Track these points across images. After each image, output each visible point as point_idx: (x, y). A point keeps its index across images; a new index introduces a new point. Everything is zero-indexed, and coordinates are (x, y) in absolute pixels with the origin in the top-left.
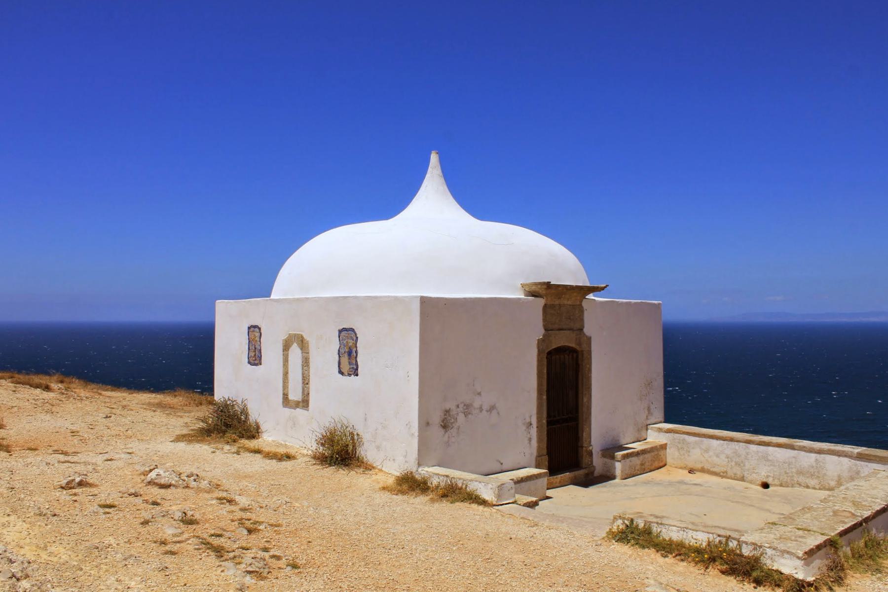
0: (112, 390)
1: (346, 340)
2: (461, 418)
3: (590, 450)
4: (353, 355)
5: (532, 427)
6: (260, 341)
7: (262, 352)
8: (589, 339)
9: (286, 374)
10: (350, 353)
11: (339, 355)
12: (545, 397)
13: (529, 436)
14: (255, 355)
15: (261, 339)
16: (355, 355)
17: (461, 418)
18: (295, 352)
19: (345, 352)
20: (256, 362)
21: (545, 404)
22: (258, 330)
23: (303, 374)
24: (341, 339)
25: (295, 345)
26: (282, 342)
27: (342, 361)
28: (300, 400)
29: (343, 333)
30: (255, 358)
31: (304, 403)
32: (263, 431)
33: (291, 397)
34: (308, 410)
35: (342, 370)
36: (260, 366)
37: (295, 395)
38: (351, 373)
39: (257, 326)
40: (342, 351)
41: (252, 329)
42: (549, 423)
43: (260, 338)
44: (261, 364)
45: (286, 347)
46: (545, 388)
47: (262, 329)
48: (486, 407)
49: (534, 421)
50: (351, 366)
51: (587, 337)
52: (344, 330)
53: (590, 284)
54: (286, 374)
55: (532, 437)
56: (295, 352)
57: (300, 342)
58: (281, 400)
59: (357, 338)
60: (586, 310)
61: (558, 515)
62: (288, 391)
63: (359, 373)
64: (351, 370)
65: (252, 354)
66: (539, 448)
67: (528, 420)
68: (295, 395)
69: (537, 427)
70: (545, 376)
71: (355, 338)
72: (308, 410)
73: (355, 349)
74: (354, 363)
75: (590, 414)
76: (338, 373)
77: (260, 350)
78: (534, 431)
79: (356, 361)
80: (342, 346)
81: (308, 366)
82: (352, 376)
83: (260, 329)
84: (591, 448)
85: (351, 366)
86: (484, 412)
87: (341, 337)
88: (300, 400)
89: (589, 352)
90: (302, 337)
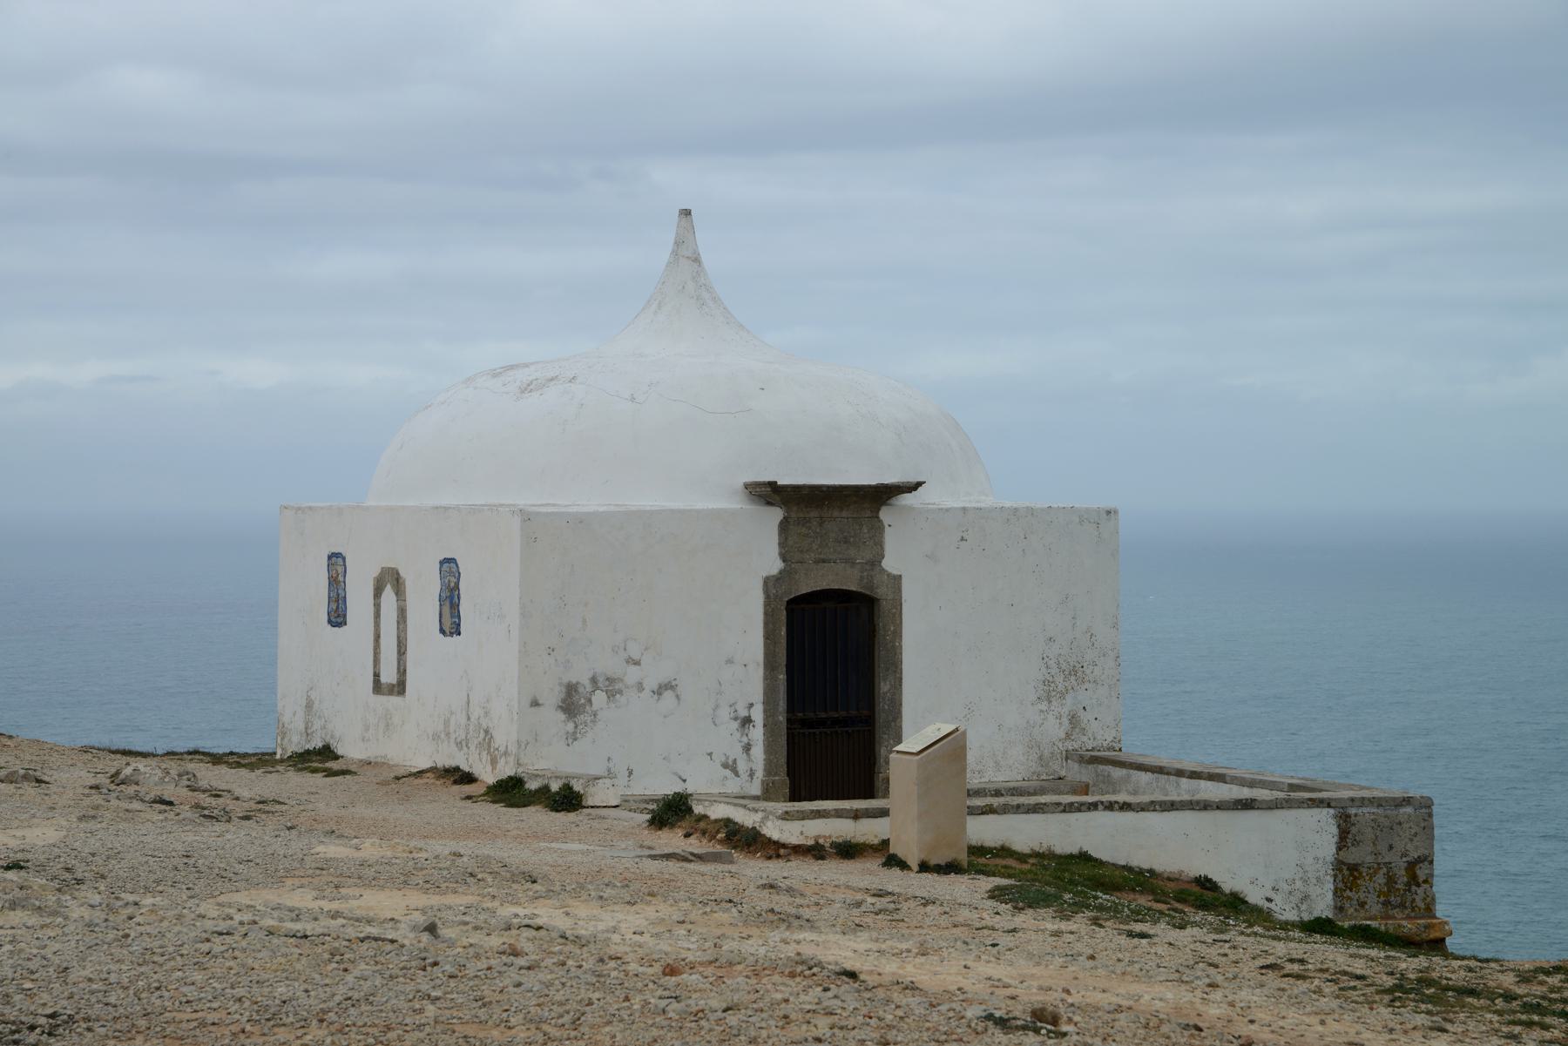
2: (599, 698)
5: (754, 726)
6: (345, 582)
8: (897, 579)
9: (377, 637)
10: (451, 597)
12: (782, 677)
13: (745, 740)
14: (338, 607)
17: (599, 698)
18: (389, 595)
20: (339, 620)
22: (340, 560)
23: (398, 637)
26: (372, 583)
27: (443, 611)
28: (395, 682)
30: (337, 618)
31: (400, 688)
32: (584, 804)
33: (384, 679)
36: (345, 627)
37: (389, 676)
39: (340, 554)
41: (334, 559)
43: (345, 576)
44: (345, 624)
45: (378, 592)
46: (782, 659)
47: (347, 560)
48: (651, 683)
49: (758, 715)
51: (889, 575)
54: (377, 637)
55: (751, 743)
56: (389, 595)
57: (395, 583)
58: (371, 685)
61: (379, 760)
62: (379, 669)
64: (453, 626)
65: (334, 606)
66: (769, 769)
67: (743, 713)
69: (765, 726)
70: (784, 642)
72: (889, 839)
77: (345, 597)
78: (757, 734)
79: (459, 612)
83: (344, 559)
86: (647, 692)
88: (395, 682)
89: (898, 604)
90: (398, 574)
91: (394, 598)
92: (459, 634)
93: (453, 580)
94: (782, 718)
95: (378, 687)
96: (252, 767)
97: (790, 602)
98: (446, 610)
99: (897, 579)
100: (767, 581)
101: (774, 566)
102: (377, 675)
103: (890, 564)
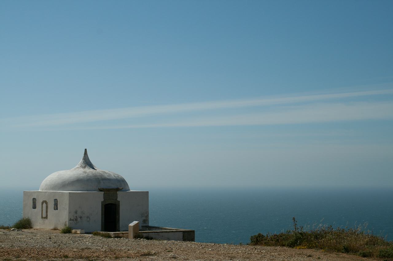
9: (42, 211)
18: (44, 205)
25: (44, 203)
30: (34, 207)
31: (46, 217)
33: (43, 216)
37: (44, 216)
54: (42, 211)
65: (34, 206)
89: (119, 205)
91: (45, 205)
92: (57, 210)
93: (56, 202)
94: (104, 221)
95: (42, 217)
96: (292, 245)
97: (54, 200)
98: (55, 206)
99: (119, 201)
100: (102, 202)
101: (103, 200)
102: (42, 216)
103: (118, 199)
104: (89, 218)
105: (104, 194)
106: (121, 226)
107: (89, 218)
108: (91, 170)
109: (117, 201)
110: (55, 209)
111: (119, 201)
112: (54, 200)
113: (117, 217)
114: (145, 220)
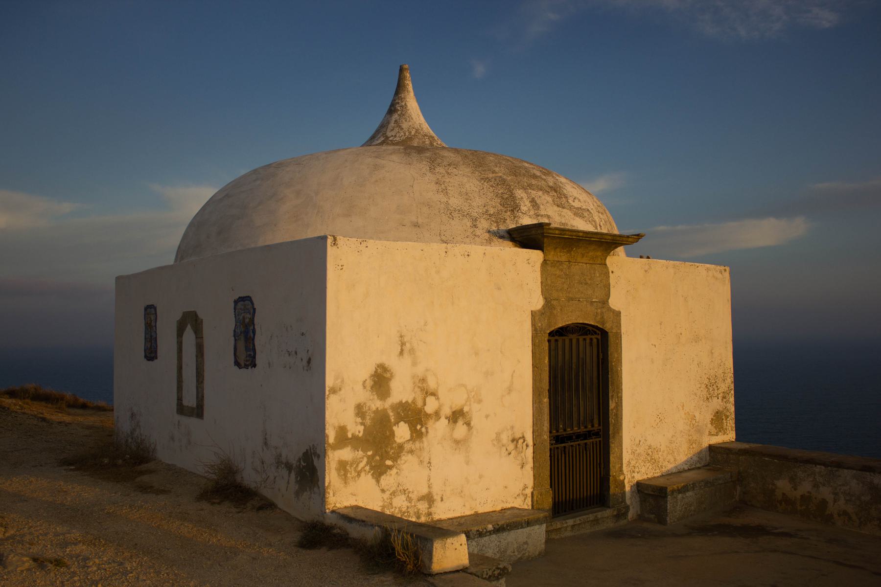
0: (724, 443)
1: (243, 314)
3: (621, 481)
4: (250, 337)
6: (156, 326)
7: (158, 340)
8: (618, 314)
10: (246, 333)
11: (235, 338)
12: (546, 400)
15: (158, 323)
16: (252, 335)
18: (189, 335)
19: (241, 333)
21: (546, 410)
24: (237, 313)
25: (189, 326)
28: (195, 406)
29: (240, 305)
31: (198, 411)
33: (185, 403)
34: (203, 419)
35: (239, 361)
37: (190, 400)
38: (248, 363)
40: (238, 331)
42: (557, 439)
50: (249, 353)
52: (242, 299)
53: (619, 229)
56: (189, 335)
59: (254, 309)
60: (612, 272)
63: (257, 362)
64: (248, 358)
68: (190, 400)
71: (252, 311)
73: (252, 328)
74: (251, 348)
75: (621, 425)
76: (233, 364)
77: (156, 338)
80: (238, 324)
81: (202, 355)
82: (250, 367)
83: (155, 309)
84: (622, 478)
85: (249, 353)
87: (237, 311)
92: (255, 366)
94: (546, 437)
95: (181, 409)
98: (241, 344)
100: (533, 314)
101: (538, 303)
102: (180, 399)
103: (615, 302)
104: (468, 424)
105: (545, 262)
106: (626, 457)
107: (468, 424)
108: (367, 382)
109: (610, 309)
110: (242, 360)
111: (235, 365)
112: (236, 302)
113: (612, 405)
114: (722, 412)
